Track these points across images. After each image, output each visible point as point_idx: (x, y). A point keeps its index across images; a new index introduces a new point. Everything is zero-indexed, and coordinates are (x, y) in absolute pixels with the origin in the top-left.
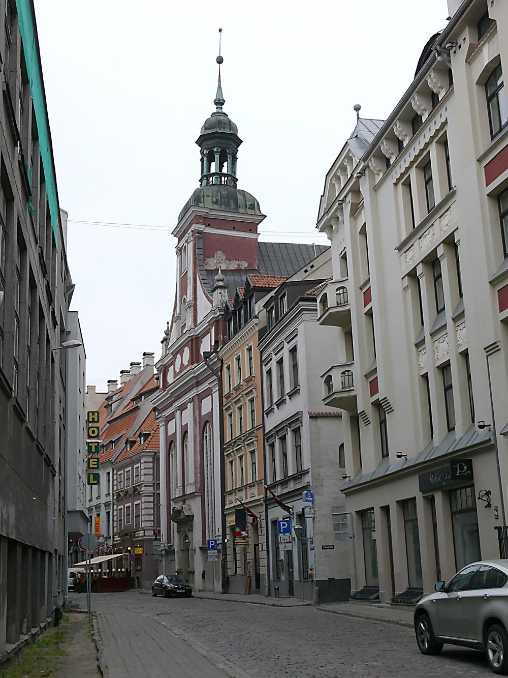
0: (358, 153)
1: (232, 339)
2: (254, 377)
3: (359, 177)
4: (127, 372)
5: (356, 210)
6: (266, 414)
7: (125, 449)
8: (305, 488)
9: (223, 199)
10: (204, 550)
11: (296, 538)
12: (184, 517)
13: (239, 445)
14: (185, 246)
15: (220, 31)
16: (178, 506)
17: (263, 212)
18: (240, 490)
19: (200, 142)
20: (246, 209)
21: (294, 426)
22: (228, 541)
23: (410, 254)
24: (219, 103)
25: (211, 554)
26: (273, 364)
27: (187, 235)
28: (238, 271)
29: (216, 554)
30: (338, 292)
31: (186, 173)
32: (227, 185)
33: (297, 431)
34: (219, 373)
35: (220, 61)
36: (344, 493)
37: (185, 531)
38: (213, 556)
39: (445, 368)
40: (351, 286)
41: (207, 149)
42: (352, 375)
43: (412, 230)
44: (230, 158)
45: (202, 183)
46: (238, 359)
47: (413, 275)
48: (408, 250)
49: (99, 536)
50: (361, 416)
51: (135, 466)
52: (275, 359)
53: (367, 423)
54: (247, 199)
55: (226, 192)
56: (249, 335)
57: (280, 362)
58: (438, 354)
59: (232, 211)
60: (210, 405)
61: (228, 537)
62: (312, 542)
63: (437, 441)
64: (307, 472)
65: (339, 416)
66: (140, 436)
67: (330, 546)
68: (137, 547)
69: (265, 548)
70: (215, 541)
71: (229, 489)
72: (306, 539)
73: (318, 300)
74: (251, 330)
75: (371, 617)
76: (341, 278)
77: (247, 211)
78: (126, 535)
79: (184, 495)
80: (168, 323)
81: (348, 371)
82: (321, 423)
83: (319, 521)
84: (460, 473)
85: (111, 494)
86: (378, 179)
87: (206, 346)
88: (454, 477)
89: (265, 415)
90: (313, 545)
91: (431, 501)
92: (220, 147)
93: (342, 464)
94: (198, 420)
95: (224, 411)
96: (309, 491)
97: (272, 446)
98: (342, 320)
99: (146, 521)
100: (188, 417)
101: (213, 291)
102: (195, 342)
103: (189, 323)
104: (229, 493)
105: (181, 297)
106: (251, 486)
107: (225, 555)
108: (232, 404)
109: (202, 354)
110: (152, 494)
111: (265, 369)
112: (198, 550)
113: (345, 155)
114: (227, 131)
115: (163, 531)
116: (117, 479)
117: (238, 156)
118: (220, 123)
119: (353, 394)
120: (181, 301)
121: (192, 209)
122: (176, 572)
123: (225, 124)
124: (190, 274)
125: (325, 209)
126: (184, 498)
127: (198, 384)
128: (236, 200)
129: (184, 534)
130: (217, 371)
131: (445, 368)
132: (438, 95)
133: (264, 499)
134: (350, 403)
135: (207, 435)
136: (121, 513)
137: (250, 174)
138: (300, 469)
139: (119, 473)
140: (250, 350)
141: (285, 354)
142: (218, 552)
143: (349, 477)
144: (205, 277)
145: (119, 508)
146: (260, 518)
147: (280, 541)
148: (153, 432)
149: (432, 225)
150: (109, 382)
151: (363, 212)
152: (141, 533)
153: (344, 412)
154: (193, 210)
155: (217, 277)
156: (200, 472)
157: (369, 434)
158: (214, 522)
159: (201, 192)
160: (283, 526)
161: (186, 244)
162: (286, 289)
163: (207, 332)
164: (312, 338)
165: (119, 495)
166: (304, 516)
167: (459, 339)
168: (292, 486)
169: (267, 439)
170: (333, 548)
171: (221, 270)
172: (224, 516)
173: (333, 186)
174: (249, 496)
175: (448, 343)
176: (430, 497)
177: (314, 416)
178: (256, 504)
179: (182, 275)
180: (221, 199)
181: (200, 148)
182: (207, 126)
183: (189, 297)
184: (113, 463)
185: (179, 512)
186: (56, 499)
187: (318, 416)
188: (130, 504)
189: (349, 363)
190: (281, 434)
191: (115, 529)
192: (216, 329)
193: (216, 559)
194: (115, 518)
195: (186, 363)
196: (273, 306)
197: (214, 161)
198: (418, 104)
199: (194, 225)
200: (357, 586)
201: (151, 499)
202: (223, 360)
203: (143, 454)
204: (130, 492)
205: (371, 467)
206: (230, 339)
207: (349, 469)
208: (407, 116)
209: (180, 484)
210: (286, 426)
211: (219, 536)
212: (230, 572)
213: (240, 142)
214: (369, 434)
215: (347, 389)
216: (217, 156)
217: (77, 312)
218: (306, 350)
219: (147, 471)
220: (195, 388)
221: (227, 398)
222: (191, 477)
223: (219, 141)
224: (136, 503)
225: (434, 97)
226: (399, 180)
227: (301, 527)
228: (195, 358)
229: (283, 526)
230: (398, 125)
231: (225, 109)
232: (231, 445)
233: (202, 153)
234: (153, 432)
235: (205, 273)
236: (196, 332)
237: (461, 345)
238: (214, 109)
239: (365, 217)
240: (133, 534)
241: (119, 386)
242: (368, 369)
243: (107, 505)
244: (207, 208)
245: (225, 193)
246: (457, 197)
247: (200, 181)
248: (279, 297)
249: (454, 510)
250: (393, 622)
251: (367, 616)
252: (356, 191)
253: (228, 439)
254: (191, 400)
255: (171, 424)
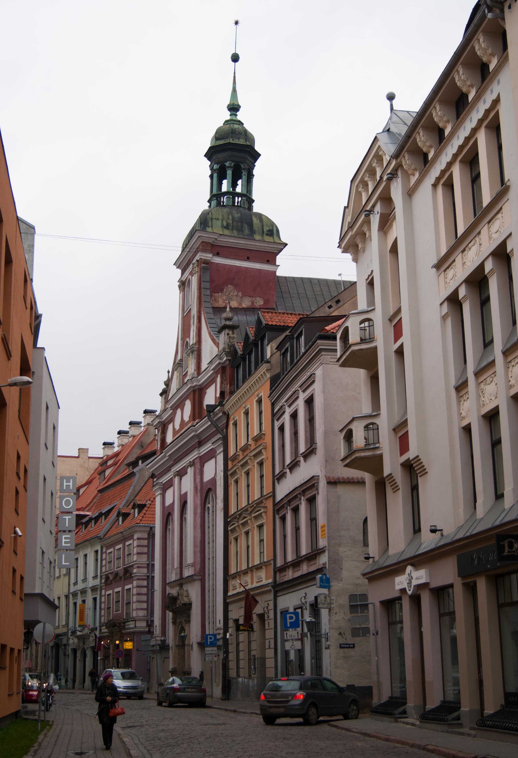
0: (389, 149)
1: (240, 387)
2: (264, 434)
3: (389, 179)
4: (127, 432)
5: (386, 222)
6: (277, 479)
7: (117, 523)
8: (320, 570)
9: (235, 224)
10: (202, 645)
11: (309, 633)
12: (181, 605)
13: (245, 517)
14: (189, 279)
15: (237, 23)
16: (174, 591)
17: (284, 239)
18: (245, 572)
19: (210, 154)
20: (263, 236)
21: (309, 495)
22: (231, 635)
23: (450, 273)
24: (234, 108)
25: (209, 652)
26: (286, 418)
27: (191, 266)
28: (252, 309)
29: (216, 652)
30: (363, 325)
31: (193, 189)
32: (240, 206)
33: (312, 501)
34: (225, 430)
35: (235, 58)
36: (367, 578)
37: (181, 623)
38: (211, 654)
39: (492, 417)
40: (378, 317)
41: (218, 164)
42: (378, 429)
43: (453, 241)
44: (245, 175)
45: (210, 204)
46: (247, 413)
47: (454, 300)
48: (448, 268)
49: (83, 626)
50: (390, 483)
51: (127, 543)
52: (288, 411)
53: (395, 489)
54: (264, 224)
55: (239, 215)
56: (258, 385)
57: (294, 416)
58: (483, 399)
59: (246, 237)
60: (213, 469)
61: (230, 630)
62: (327, 638)
63: (480, 512)
64: (322, 551)
65: (361, 483)
66: (134, 508)
67: (349, 644)
68: (127, 641)
69: (272, 646)
70: (215, 635)
71: (233, 570)
72: (321, 635)
73: (338, 336)
74: (262, 374)
75: (392, 738)
76: (368, 307)
77: (265, 240)
78: (114, 625)
79: (181, 578)
80: (169, 372)
81: (373, 424)
82: (341, 490)
83: (336, 613)
84: (509, 552)
85: (99, 577)
86: (413, 180)
87: (210, 398)
88: (501, 558)
89: (276, 481)
90: (329, 643)
91: (471, 589)
92: (233, 161)
93: (366, 544)
94: (199, 487)
95: (229, 477)
96: (325, 574)
97: (283, 519)
98: (364, 359)
99: (137, 610)
100: (187, 484)
101: (220, 332)
102: (197, 393)
103: (191, 369)
104: (233, 576)
105: (183, 339)
106: (258, 568)
107: (227, 652)
108: (238, 468)
109: (205, 408)
110: (146, 578)
111: (277, 424)
112: (195, 647)
113: (374, 153)
114: (242, 142)
115: (157, 622)
116: (106, 559)
117: (255, 172)
118: (233, 133)
119: (378, 452)
120: (183, 345)
121: (197, 234)
122: (170, 672)
123: (240, 133)
124: (194, 312)
125: (349, 223)
126: (181, 582)
127: (200, 444)
128: (251, 225)
129: (180, 626)
130: (221, 428)
131: (492, 417)
132: (488, 66)
133: (273, 584)
134: (373, 463)
135: (210, 506)
136: (109, 600)
137: (269, 193)
138: (314, 548)
139: (108, 551)
140: (260, 401)
141: (300, 405)
142: (218, 649)
143: (373, 558)
144: (212, 316)
145: (108, 593)
146: (267, 608)
147: (286, 638)
148: (149, 502)
149: (479, 233)
150: (104, 444)
151: (394, 224)
152: (131, 625)
153: (367, 477)
154: (199, 235)
155: (224, 315)
156: (201, 550)
157: (397, 504)
158: (214, 612)
159: (208, 214)
160: (290, 619)
161: (190, 277)
162: (303, 326)
163: (211, 381)
164: (333, 387)
165: (107, 578)
166: (317, 606)
167: (510, 379)
168: (305, 569)
169: (278, 511)
170: (354, 647)
171: (230, 308)
172: (226, 605)
173: (359, 195)
174: (255, 580)
175: (496, 384)
176: (472, 584)
177: (332, 481)
178: (262, 590)
179: (185, 314)
180: (233, 223)
181: (209, 163)
182: (219, 135)
183: (192, 340)
184: (102, 539)
185: (174, 599)
186: (44, 580)
187: (337, 481)
188: (120, 589)
189: (374, 414)
190: (294, 504)
191: (103, 618)
192: (222, 378)
193: (216, 659)
194: (103, 605)
195: (186, 418)
196: (288, 347)
197: (226, 179)
198: (462, 78)
199: (199, 254)
200: (383, 694)
201: (145, 583)
202: (229, 415)
203: (137, 529)
204: (121, 574)
205: (399, 543)
206: (238, 388)
207: (373, 549)
208: (450, 96)
209: (176, 564)
210: (300, 494)
211: (220, 629)
212: (232, 673)
213: (256, 156)
214: (397, 504)
215: (372, 447)
216: (229, 173)
217: (44, 348)
218: (325, 399)
219: (140, 550)
220: (196, 450)
221: (233, 461)
222: (190, 557)
223: (233, 154)
224: (127, 587)
225: (484, 68)
226: (438, 179)
227: (313, 620)
228: (198, 412)
229: (290, 619)
230: (438, 108)
231: (240, 116)
232: (235, 518)
233: (212, 169)
234: (149, 502)
235: (211, 310)
236: (199, 382)
237: (514, 386)
238: (227, 115)
239: (398, 230)
240: (123, 625)
241: (116, 449)
242: (397, 420)
243: (94, 589)
244: (216, 232)
245: (237, 215)
246: (512, 194)
247: (208, 201)
248: (295, 336)
249: (502, 601)
250: (419, 747)
251: (387, 737)
252: (386, 199)
253: (233, 510)
254: (192, 463)
255: (169, 494)
